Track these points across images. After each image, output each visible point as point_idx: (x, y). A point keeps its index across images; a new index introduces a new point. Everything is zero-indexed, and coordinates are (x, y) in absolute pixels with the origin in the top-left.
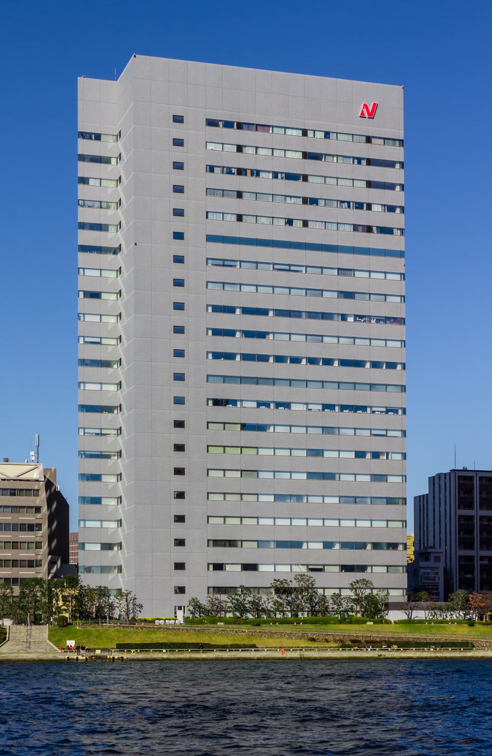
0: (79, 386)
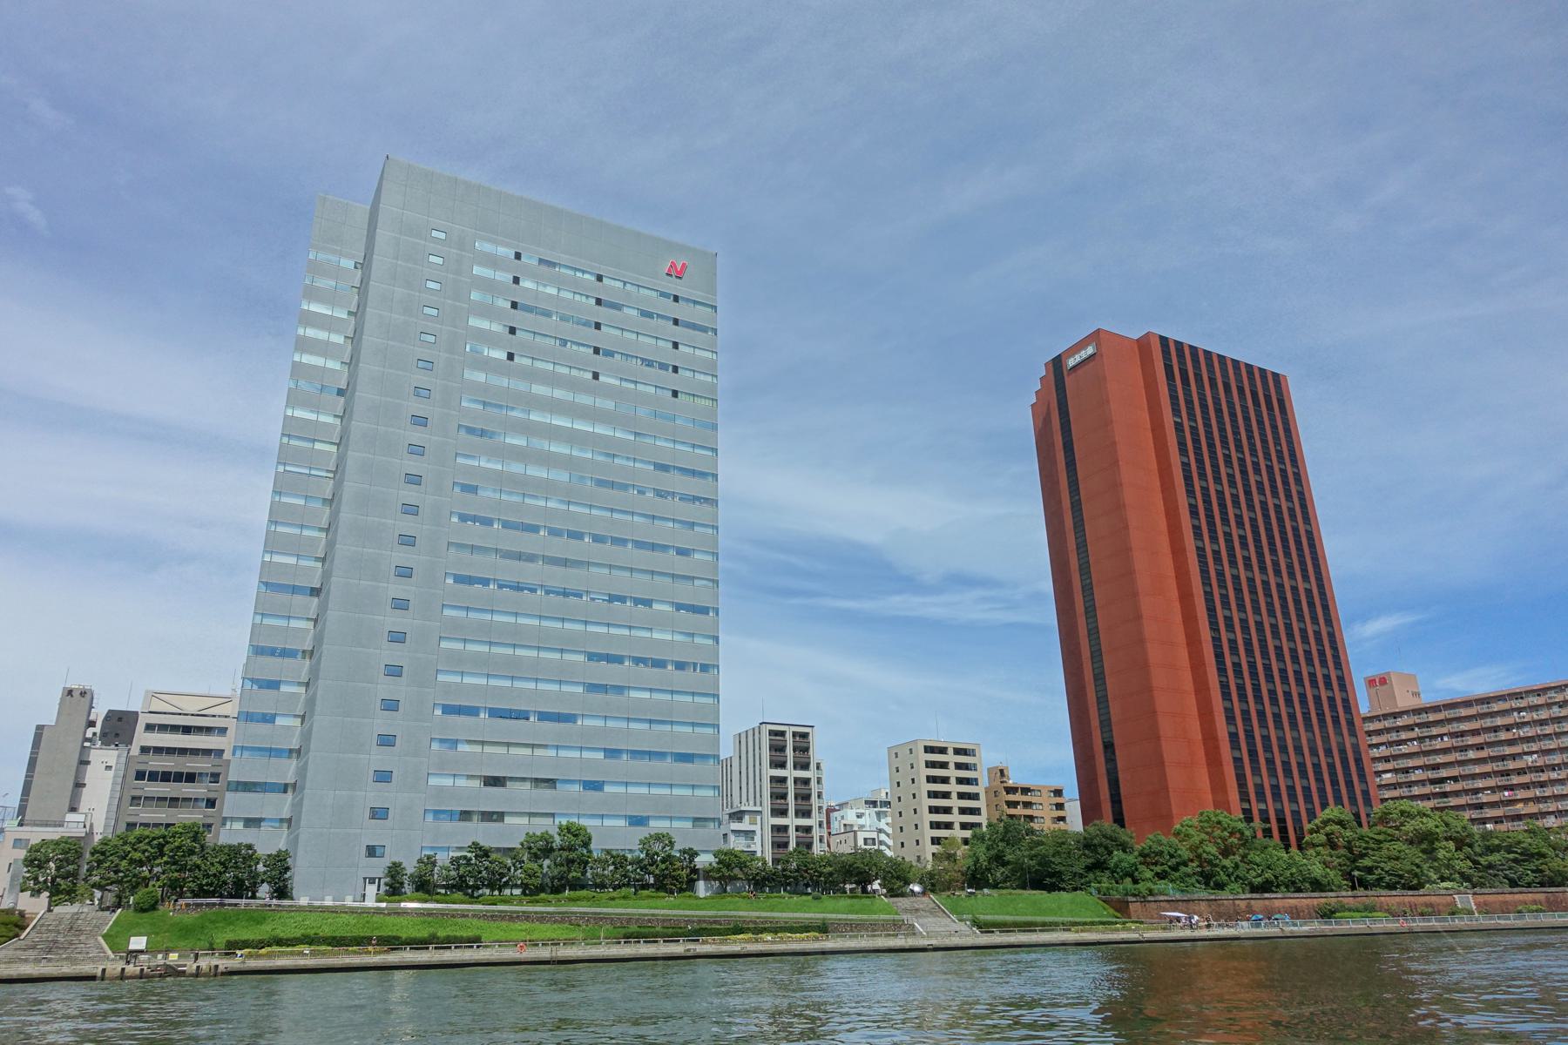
0: (224, 824)
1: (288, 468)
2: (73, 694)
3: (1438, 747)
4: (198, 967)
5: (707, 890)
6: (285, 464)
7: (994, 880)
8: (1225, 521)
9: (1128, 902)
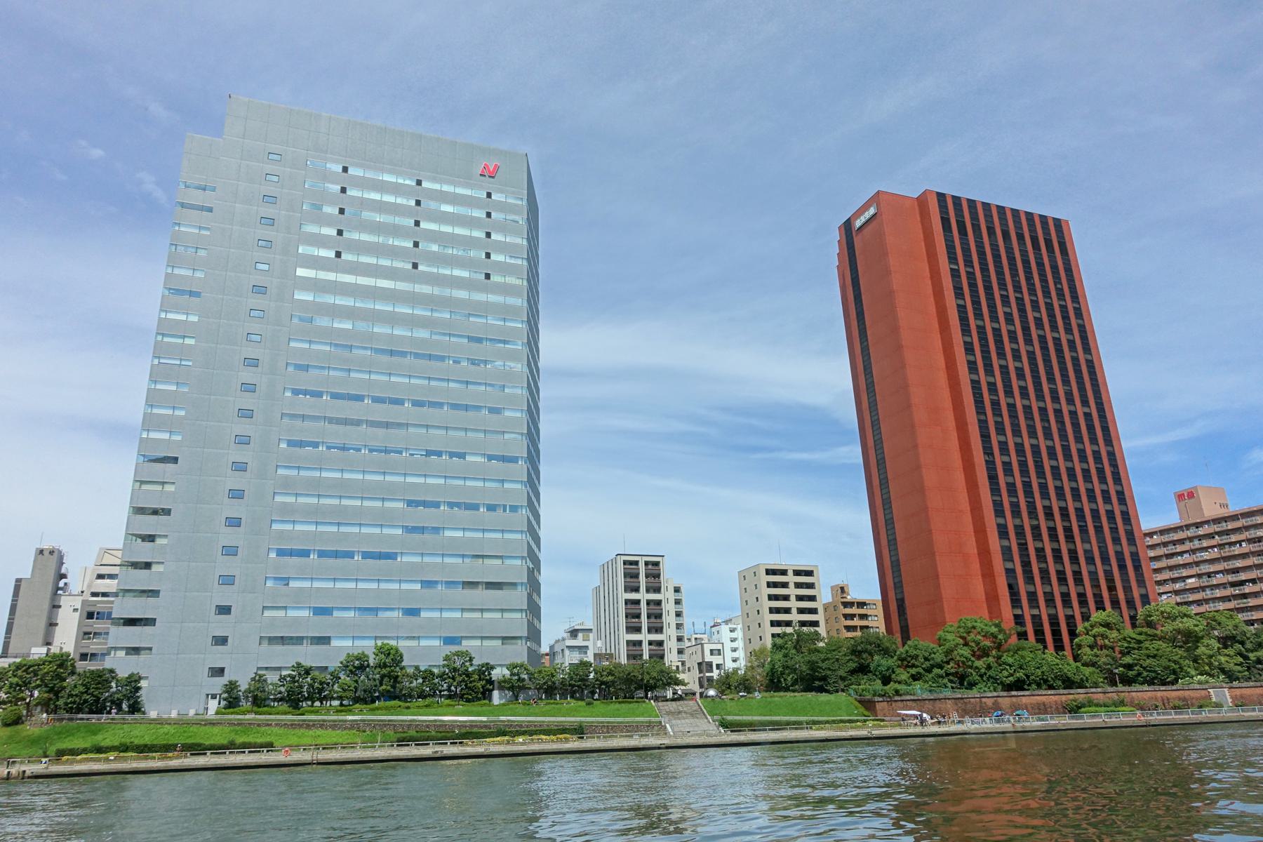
1: (162, 361)
2: (44, 552)
3: (1236, 553)
4: (9, 772)
5: (500, 699)
6: (159, 358)
7: (786, 684)
8: (1001, 354)
9: (875, 702)
